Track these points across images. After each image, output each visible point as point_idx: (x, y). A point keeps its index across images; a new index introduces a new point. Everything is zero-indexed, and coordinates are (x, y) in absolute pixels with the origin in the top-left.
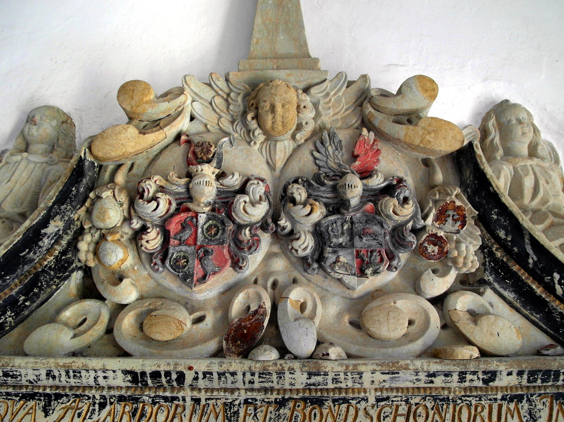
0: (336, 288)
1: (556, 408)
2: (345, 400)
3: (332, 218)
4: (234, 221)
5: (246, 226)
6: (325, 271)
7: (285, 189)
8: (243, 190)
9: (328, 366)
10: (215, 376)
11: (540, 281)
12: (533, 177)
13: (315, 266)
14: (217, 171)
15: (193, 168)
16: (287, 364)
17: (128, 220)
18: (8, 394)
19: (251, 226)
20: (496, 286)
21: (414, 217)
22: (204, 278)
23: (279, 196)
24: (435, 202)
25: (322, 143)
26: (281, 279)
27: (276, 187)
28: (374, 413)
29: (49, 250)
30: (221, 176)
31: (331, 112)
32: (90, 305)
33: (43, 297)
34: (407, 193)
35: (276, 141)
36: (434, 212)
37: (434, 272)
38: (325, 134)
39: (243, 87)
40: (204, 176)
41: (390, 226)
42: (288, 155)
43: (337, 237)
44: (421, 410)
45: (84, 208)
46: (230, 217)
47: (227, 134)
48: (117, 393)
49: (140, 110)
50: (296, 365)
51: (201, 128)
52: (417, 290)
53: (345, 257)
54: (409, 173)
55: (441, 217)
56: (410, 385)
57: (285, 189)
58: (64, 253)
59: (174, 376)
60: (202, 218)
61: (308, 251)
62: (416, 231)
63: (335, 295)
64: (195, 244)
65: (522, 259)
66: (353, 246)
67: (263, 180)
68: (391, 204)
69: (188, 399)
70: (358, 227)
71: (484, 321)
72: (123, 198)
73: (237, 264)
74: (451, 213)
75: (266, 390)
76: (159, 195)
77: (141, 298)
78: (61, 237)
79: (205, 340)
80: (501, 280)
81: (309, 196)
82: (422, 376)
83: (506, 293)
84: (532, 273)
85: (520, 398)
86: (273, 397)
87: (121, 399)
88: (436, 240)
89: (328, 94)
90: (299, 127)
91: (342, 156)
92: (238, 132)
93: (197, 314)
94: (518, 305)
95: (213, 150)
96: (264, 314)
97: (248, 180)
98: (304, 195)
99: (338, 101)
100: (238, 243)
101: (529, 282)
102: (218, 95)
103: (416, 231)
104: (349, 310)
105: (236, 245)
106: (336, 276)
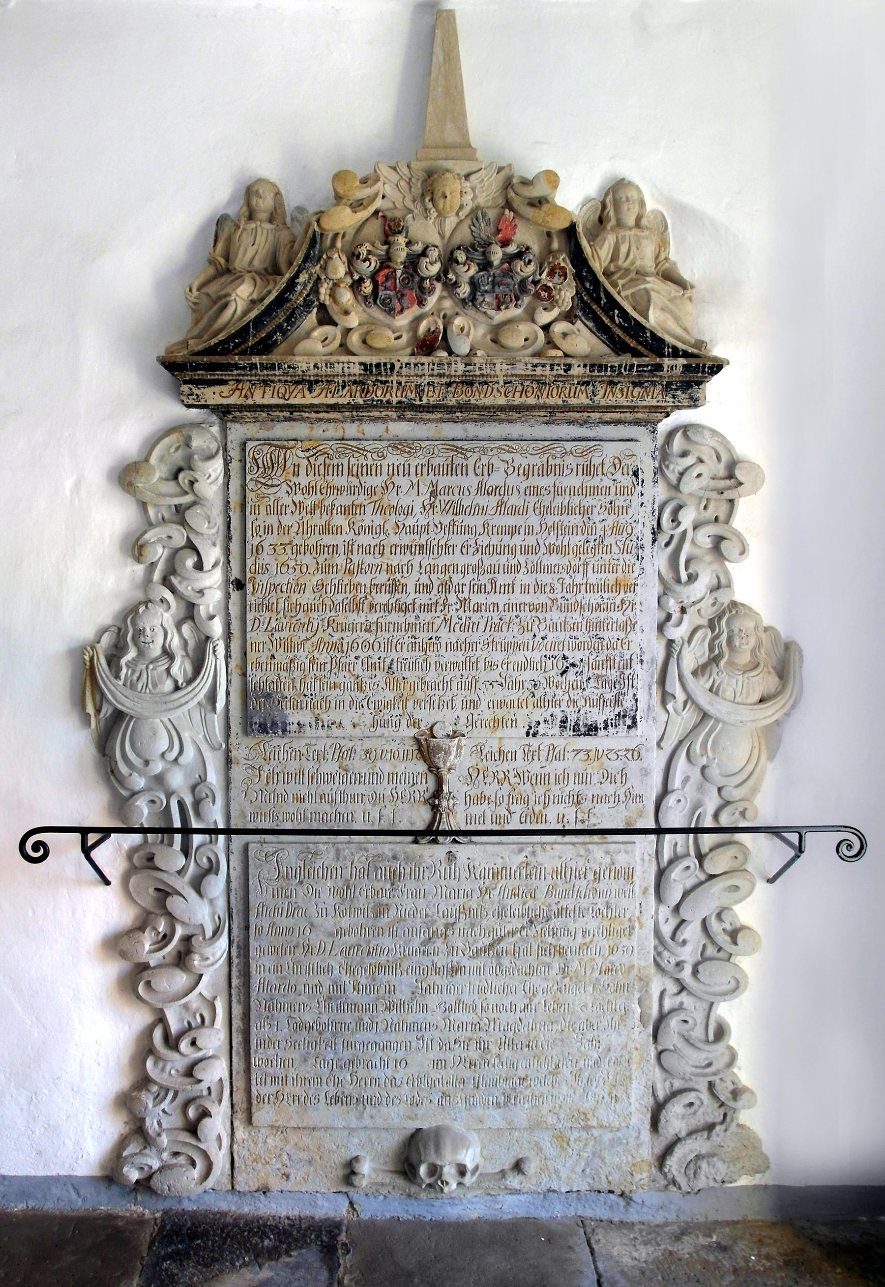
0: (482, 318)
1: (609, 390)
2: (486, 383)
3: (481, 273)
4: (418, 274)
5: (427, 278)
6: (476, 307)
7: (452, 253)
8: (424, 254)
9: (476, 360)
10: (412, 365)
11: (607, 314)
12: (628, 245)
13: (470, 304)
14: (407, 240)
15: (391, 239)
16: (453, 359)
17: (350, 273)
18: (286, 381)
19: (430, 278)
20: (583, 318)
21: (534, 273)
22: (402, 311)
23: (447, 258)
24: (549, 263)
25: (477, 219)
26: (449, 313)
27: (445, 251)
28: (502, 390)
29: (301, 294)
30: (409, 244)
31: (484, 194)
32: (328, 329)
33: (298, 324)
34: (531, 257)
35: (445, 217)
36: (547, 270)
37: (545, 309)
38: (480, 213)
39: (422, 175)
40: (400, 244)
41: (518, 279)
42: (453, 227)
43: (484, 286)
44: (529, 389)
45: (319, 265)
46: (415, 271)
47: (411, 211)
48: (352, 378)
49: (350, 193)
50: (458, 359)
51: (391, 205)
52: (533, 321)
53: (488, 299)
54: (536, 241)
55: (551, 274)
56: (523, 373)
57: (452, 253)
58: (308, 295)
59: (389, 366)
60: (399, 273)
61: (466, 295)
62: (535, 283)
63: (482, 323)
64: (395, 289)
65: (597, 301)
66: (494, 292)
67: (437, 247)
68: (519, 265)
69: (395, 382)
70: (498, 279)
71: (569, 338)
72: (344, 258)
73: (421, 303)
74: (557, 271)
75: (440, 375)
76: (370, 257)
77: (360, 324)
78: (306, 285)
79: (403, 348)
80: (586, 315)
81: (467, 258)
82: (529, 366)
83: (588, 323)
84: (603, 309)
85: (588, 383)
86: (445, 380)
87: (355, 382)
88: (547, 288)
89: (483, 180)
90: (461, 207)
91: (491, 229)
92: (418, 210)
93: (397, 334)
94: (594, 330)
95: (402, 224)
96: (439, 332)
97: (427, 247)
98: (464, 258)
99: (490, 185)
100: (422, 289)
101: (602, 316)
102: (402, 178)
103: (535, 283)
104: (490, 332)
105: (420, 290)
106: (483, 310)
